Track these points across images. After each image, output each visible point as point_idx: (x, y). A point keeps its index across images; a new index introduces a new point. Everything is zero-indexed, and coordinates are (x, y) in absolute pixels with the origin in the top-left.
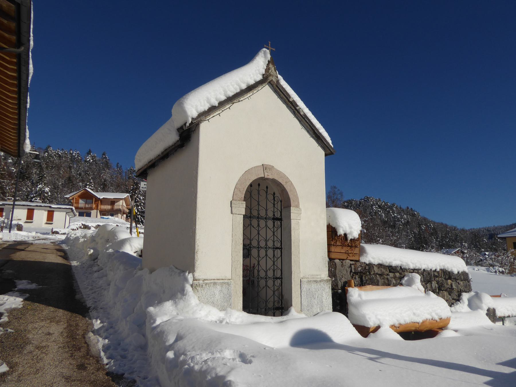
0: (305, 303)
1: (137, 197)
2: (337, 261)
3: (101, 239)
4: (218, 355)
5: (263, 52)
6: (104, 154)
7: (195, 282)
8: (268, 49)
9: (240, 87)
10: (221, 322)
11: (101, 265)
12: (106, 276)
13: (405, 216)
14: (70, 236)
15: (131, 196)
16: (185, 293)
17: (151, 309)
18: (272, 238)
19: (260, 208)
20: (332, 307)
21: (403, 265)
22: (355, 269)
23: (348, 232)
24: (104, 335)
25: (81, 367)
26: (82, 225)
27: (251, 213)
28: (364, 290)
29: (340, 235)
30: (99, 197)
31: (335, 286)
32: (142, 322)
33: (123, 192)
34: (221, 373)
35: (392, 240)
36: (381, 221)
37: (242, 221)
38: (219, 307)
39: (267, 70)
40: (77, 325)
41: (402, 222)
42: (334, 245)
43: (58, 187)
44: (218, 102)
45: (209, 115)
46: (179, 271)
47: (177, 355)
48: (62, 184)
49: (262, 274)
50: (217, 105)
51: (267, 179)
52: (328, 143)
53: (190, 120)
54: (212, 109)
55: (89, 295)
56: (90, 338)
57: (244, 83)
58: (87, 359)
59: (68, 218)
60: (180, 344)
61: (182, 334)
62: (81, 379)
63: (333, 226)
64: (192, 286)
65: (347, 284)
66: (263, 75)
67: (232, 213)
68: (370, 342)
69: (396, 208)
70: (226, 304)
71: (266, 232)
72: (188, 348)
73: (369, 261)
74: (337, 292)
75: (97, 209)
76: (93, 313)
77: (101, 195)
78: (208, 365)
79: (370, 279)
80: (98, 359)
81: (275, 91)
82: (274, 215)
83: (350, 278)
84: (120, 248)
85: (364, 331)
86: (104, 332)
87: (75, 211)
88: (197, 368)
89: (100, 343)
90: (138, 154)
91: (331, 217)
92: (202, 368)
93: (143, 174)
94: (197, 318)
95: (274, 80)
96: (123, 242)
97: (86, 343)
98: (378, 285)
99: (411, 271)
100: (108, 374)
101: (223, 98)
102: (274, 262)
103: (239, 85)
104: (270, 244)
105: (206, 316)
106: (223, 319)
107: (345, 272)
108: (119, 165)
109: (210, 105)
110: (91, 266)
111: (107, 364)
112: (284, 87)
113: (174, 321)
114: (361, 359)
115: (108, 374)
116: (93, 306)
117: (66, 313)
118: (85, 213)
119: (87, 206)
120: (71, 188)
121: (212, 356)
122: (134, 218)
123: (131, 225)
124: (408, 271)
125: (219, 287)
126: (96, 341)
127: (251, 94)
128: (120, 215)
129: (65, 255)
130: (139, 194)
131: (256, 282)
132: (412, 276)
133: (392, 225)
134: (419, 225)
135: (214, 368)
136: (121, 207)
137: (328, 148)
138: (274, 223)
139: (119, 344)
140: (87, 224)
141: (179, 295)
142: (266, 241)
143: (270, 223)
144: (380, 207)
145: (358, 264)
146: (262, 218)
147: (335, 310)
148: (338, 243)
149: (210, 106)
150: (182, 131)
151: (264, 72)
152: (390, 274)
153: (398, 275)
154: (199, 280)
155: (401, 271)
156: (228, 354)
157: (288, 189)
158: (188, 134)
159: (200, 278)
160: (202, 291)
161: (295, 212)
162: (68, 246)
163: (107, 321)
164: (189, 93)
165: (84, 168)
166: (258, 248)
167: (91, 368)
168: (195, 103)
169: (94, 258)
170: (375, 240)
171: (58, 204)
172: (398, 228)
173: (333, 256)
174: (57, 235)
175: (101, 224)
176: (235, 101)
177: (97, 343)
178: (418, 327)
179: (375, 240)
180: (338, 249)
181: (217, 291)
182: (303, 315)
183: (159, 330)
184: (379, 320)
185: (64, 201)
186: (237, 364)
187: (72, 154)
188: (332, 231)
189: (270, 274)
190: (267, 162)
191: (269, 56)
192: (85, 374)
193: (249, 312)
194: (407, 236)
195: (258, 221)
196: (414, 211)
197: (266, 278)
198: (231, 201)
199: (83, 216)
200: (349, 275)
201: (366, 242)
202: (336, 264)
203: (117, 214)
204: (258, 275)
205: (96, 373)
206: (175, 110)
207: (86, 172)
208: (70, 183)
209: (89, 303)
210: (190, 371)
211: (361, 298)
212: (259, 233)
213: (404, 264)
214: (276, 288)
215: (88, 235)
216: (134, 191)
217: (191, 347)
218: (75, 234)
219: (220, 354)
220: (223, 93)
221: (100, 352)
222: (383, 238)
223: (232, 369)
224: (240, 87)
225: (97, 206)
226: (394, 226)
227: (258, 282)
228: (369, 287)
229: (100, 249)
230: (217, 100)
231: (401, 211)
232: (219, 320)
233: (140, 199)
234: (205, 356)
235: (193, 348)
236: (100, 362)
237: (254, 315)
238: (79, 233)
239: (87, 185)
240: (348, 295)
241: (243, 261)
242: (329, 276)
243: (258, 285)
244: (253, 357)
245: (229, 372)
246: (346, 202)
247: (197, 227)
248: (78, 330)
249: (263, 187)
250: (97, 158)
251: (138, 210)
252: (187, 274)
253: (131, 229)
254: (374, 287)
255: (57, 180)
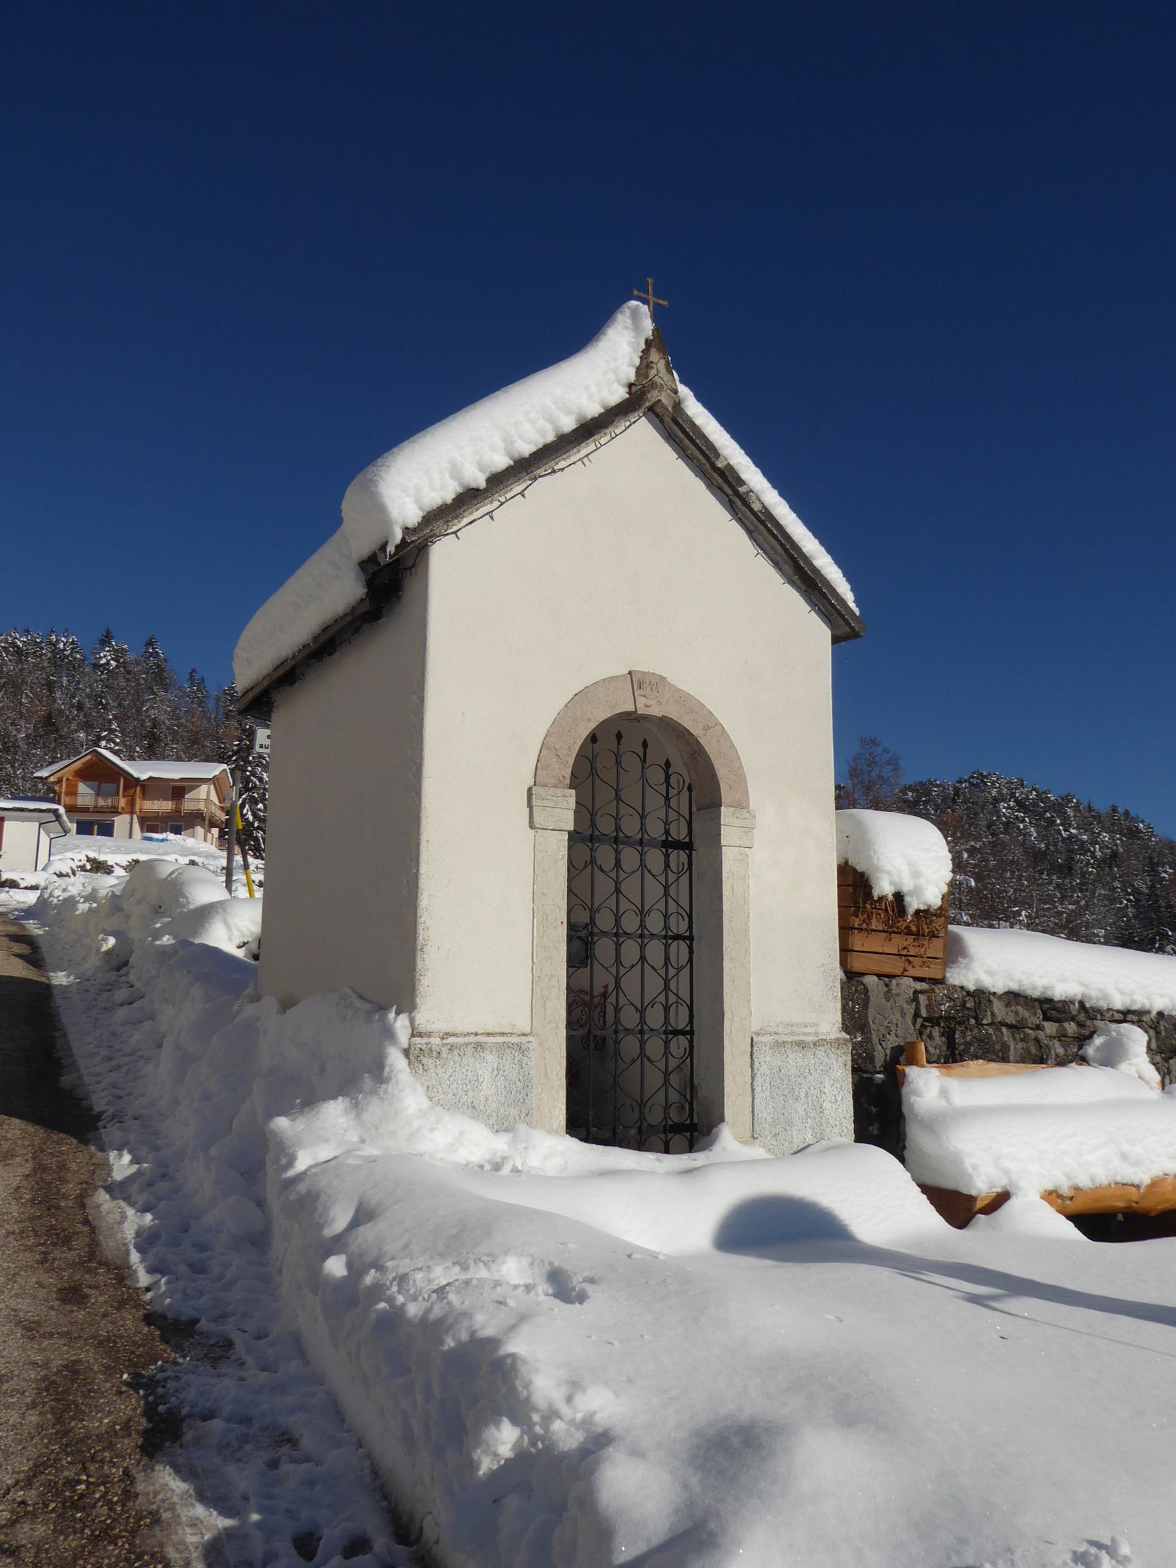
0: (764, 1111)
1: (253, 774)
2: (870, 980)
3: (139, 903)
4: (482, 1273)
5: (628, 312)
6: (150, 643)
7: (417, 1040)
8: (645, 301)
9: (556, 428)
10: (497, 1167)
11: (138, 985)
12: (153, 1018)
13: (1106, 837)
14: (51, 895)
15: (232, 770)
16: (385, 1074)
17: (281, 1123)
18: (661, 905)
19: (624, 810)
20: (852, 1127)
21: (1090, 998)
22: (929, 1007)
23: (907, 886)
24: (141, 1199)
25: (72, 1295)
26: (89, 860)
27: (593, 825)
28: (960, 1076)
29: (882, 899)
30: (136, 775)
31: (864, 1059)
32: (255, 1164)
33: (208, 759)
34: (488, 1332)
35: (1061, 913)
36: (1026, 852)
37: (564, 852)
38: (493, 1120)
39: (644, 368)
40: (62, 1167)
41: (1093, 856)
42: (860, 930)
43: (14, 746)
44: (487, 475)
45: (458, 517)
46: (367, 1006)
47: (356, 1269)
48: (28, 736)
49: (630, 1018)
50: (482, 484)
51: (645, 718)
52: (843, 602)
53: (398, 535)
54: (468, 498)
55: (99, 1074)
56: (98, 1206)
57: (568, 412)
58: (89, 1271)
59: (44, 839)
60: (367, 1233)
61: (374, 1202)
62: (68, 1333)
63: (860, 868)
64: (406, 1053)
65: (903, 1055)
66: (630, 385)
67: (532, 825)
68: (975, 1244)
69: (1076, 808)
70: (513, 1112)
71: (644, 885)
72: (391, 1248)
73: (977, 981)
74: (871, 1079)
75: (132, 812)
76: (111, 1132)
77: (142, 770)
78: (449, 1303)
79: (981, 1041)
80: (121, 1273)
81: (670, 438)
82: (667, 832)
83: (912, 1037)
84: (196, 932)
85: (956, 1206)
86: (142, 1191)
87: (65, 818)
88: (413, 1310)
89: (127, 1223)
90: (242, 642)
91: (845, 839)
92: (428, 1311)
93: (260, 703)
94: (422, 1155)
95: (665, 401)
96: (205, 913)
97: (86, 1222)
98: (1005, 1060)
99: (1118, 1017)
100: (149, 1319)
101: (502, 462)
102: (667, 982)
103: (551, 420)
104: (655, 923)
105: (452, 1147)
106: (505, 1159)
107: (896, 1017)
108: (197, 676)
109: (461, 484)
110: (109, 987)
111: (148, 1289)
112: (698, 422)
113: (351, 1161)
114: (941, 1298)
115: (149, 1319)
116: (111, 1110)
117: (31, 1128)
118: (95, 824)
119: (101, 802)
120: (54, 749)
121: (463, 1277)
122: (239, 837)
123: (230, 859)
124: (1108, 1015)
125: (491, 1058)
126: (117, 1217)
127: (592, 447)
128: (200, 830)
129: (34, 954)
130: (259, 764)
131: (610, 1044)
132: (1118, 1033)
133: (1060, 866)
134: (1152, 867)
135: (466, 1314)
136: (202, 806)
137: (842, 616)
138: (667, 856)
139: (186, 1230)
140: (102, 858)
141: (368, 1081)
142: (643, 913)
143: (655, 858)
144: (1021, 805)
145: (941, 991)
146: (628, 841)
147: (863, 1135)
148: (875, 924)
149: (460, 490)
150: (375, 568)
151: (632, 378)
152: (1046, 1024)
153: (1071, 1028)
154: (429, 1035)
155: (1082, 1017)
156: (513, 1270)
157: (709, 744)
158: (393, 578)
159: (434, 1027)
160: (440, 1071)
161: (735, 822)
162: (44, 925)
163: (150, 1157)
164: (395, 450)
165: (91, 686)
166: (616, 935)
167: (101, 1299)
168: (412, 480)
169: (119, 962)
170: (1005, 910)
171: (15, 798)
172: (1083, 875)
173: (858, 964)
174: (13, 891)
175: (143, 857)
176: (541, 471)
177: (120, 1223)
178: (1135, 1198)
179: (1005, 910)
180: (875, 943)
181: (485, 1069)
182: (758, 1152)
183: (302, 1187)
184: (1007, 1172)
185: (34, 788)
186: (538, 1304)
187: (55, 644)
188: (854, 885)
189: (655, 1018)
190: (645, 664)
191: (648, 326)
192: (81, 1315)
193: (586, 1139)
194: (1112, 901)
195: (617, 852)
196: (1136, 819)
197: (641, 1032)
198: (530, 790)
199: (92, 834)
200: (907, 1027)
201: (975, 922)
202: (866, 990)
203: (193, 827)
204: (617, 1021)
205: (116, 1315)
206: (350, 504)
207: (96, 698)
208: (51, 734)
209: (100, 1101)
210: (393, 1320)
211: (948, 1101)
212: (618, 890)
213: (1094, 993)
214: (673, 1063)
215: (103, 893)
216: (241, 757)
217: (400, 1244)
218: (64, 890)
219: (489, 1270)
220: (502, 445)
221: (128, 1252)
222: (1030, 906)
223: (523, 1318)
224: (556, 428)
225: (132, 803)
226: (1067, 869)
227: (617, 1042)
228: (974, 1065)
229: (134, 935)
230: (481, 469)
231: (1091, 818)
232: (489, 1162)
233: (261, 779)
234: (441, 1275)
235: (406, 1246)
236: (127, 1282)
237: (601, 1148)
238: (77, 886)
239: (100, 738)
240: (905, 1090)
241: (569, 976)
242: (846, 1028)
243: (617, 1053)
244: (592, 1281)
245: (513, 1328)
246: (910, 788)
247: (424, 869)
248: (65, 1181)
249: (632, 743)
250: (131, 657)
251: (254, 815)
252: (392, 1015)
253: (228, 871)
254: (992, 1065)
255: (13, 724)
